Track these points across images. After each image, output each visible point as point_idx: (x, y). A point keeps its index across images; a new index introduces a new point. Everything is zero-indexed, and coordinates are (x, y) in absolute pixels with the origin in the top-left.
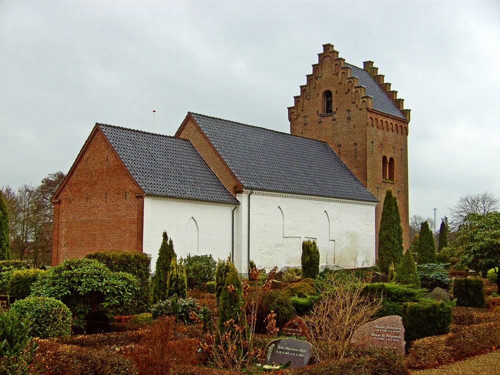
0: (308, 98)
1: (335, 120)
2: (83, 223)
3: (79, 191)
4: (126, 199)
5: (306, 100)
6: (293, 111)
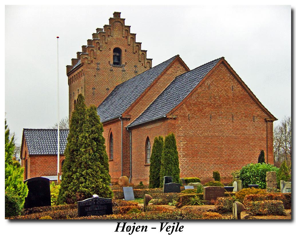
0: (101, 49)
1: (125, 71)
2: (206, 137)
3: (200, 111)
4: (254, 121)
5: (99, 51)
6: (87, 57)
